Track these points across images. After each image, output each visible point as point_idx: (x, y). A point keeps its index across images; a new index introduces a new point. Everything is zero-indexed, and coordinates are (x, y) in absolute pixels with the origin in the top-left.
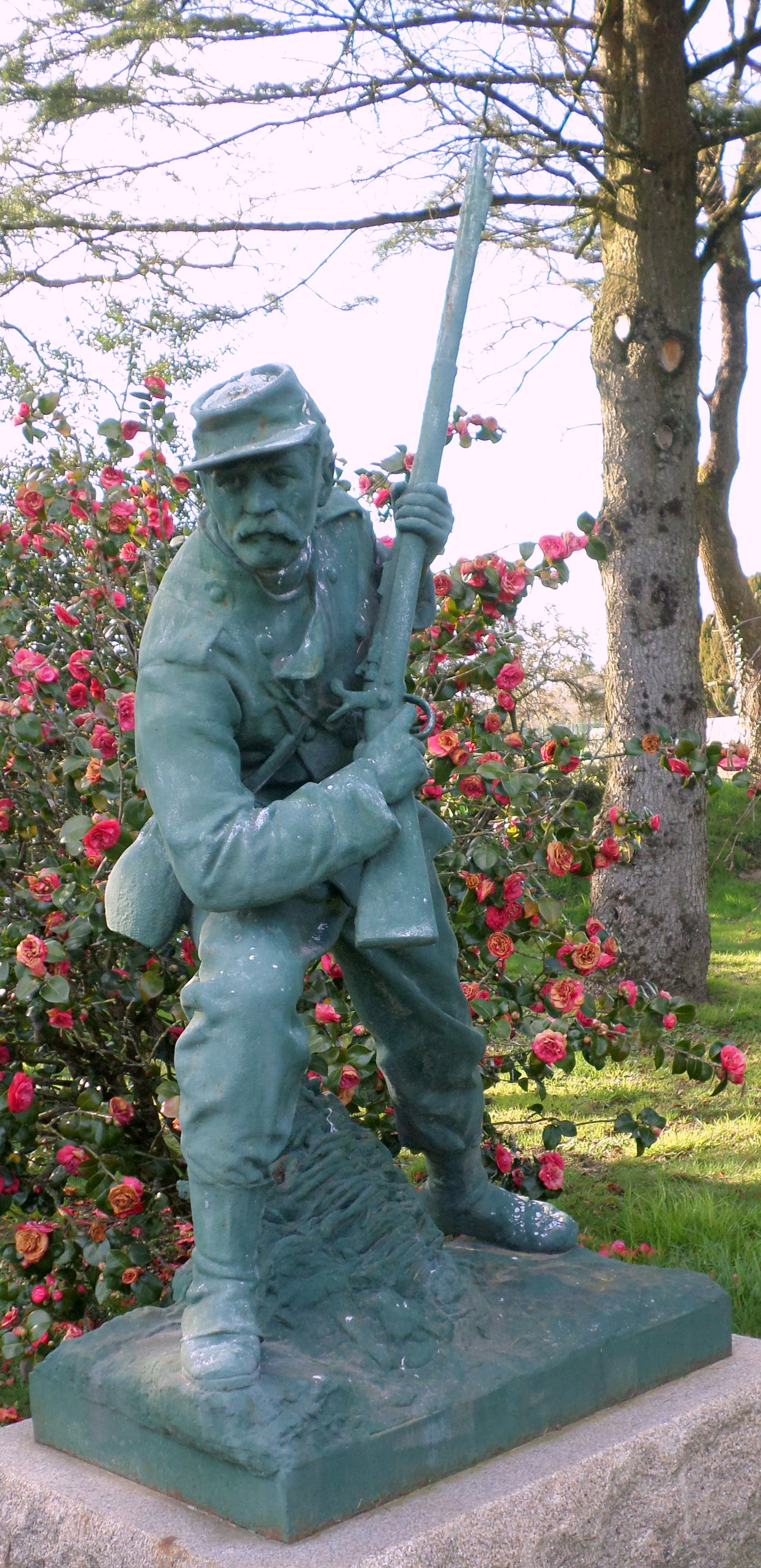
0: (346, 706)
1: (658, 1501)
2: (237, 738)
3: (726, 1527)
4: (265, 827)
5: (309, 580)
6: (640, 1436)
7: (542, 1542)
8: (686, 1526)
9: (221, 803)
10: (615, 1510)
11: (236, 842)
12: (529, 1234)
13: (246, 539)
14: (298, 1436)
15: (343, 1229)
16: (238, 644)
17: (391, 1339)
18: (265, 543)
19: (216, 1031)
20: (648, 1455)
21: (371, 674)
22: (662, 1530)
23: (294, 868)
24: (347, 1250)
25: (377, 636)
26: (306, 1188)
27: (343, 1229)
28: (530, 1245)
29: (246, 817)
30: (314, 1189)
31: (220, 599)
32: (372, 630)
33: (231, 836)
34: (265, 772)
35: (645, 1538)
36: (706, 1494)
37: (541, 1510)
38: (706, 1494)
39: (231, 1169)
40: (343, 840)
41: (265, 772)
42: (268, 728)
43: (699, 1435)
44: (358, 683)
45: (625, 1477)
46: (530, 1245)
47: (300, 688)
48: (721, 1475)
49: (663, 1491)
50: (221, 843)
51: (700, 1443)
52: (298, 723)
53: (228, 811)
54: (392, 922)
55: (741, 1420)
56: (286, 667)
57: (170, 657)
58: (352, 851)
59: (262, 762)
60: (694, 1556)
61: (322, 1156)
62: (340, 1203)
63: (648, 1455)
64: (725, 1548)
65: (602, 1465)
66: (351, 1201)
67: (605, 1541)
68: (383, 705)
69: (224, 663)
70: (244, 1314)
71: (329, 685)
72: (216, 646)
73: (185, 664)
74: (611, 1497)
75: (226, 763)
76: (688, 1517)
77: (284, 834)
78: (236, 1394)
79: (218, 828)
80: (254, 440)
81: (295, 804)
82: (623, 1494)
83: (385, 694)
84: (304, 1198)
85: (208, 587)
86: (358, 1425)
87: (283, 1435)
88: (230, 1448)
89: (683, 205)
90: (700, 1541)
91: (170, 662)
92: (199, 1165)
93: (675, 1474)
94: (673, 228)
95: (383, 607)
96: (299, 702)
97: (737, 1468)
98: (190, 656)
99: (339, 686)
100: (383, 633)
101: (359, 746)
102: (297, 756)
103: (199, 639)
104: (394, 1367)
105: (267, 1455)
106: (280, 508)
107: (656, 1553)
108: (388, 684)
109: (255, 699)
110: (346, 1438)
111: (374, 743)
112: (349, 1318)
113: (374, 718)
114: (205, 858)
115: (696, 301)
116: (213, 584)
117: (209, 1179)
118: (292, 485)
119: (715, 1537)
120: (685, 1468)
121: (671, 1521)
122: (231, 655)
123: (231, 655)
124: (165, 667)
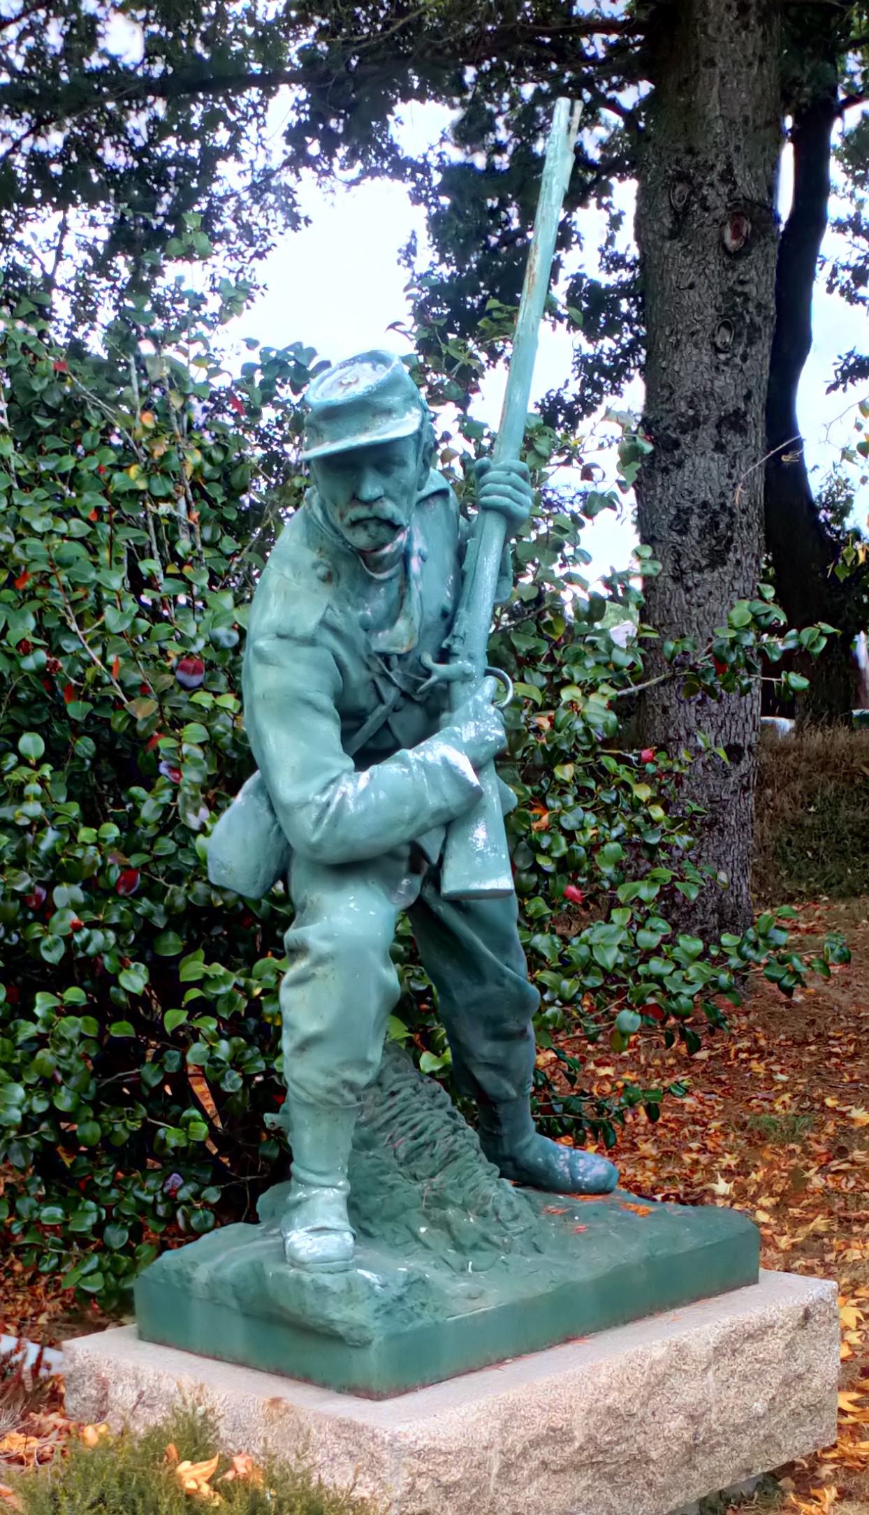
0: (434, 678)
1: (689, 1393)
2: (336, 706)
3: (748, 1424)
4: (366, 790)
5: (405, 557)
6: (675, 1337)
7: (590, 1412)
8: (714, 1417)
9: (328, 768)
10: (651, 1395)
11: (342, 804)
12: (573, 1179)
13: (355, 523)
14: (388, 1313)
15: (414, 1154)
16: (339, 621)
17: (459, 1247)
18: (373, 528)
19: (320, 970)
20: (681, 1352)
21: (456, 647)
22: (692, 1417)
23: (392, 825)
24: (419, 1173)
25: (462, 611)
26: (382, 1120)
27: (414, 1154)
28: (576, 1190)
29: (350, 780)
30: (387, 1122)
31: (327, 579)
32: (456, 603)
33: (338, 797)
34: (360, 738)
35: (676, 1423)
36: (732, 1392)
37: (591, 1387)
38: (732, 1392)
39: (331, 1091)
40: (433, 802)
41: (360, 738)
42: (364, 699)
43: (727, 1340)
44: (444, 656)
45: (660, 1369)
46: (576, 1190)
47: (394, 660)
48: (745, 1378)
49: (694, 1384)
50: (328, 804)
51: (727, 1348)
52: (390, 695)
53: (334, 775)
54: (473, 878)
55: (765, 1333)
56: (382, 641)
57: (284, 632)
58: (439, 812)
59: (358, 729)
60: (719, 1444)
61: (393, 1094)
62: (410, 1134)
63: (681, 1352)
64: (746, 1442)
65: (644, 1357)
66: (421, 1133)
67: (643, 1420)
68: (466, 677)
69: (329, 638)
70: (341, 1217)
71: (419, 659)
72: (324, 623)
73: (296, 639)
74: (648, 1383)
75: (329, 730)
76: (715, 1409)
77: (382, 795)
78: (338, 1276)
79: (324, 789)
80: (366, 430)
81: (388, 770)
82: (658, 1383)
83: (468, 665)
84: (379, 1129)
85: (315, 566)
86: (436, 1310)
87: (377, 1310)
88: (332, 1321)
89: (764, 35)
90: (725, 1432)
91: (281, 636)
92: (303, 1088)
93: (705, 1370)
94: (750, 65)
95: (468, 583)
96: (392, 675)
97: (761, 1373)
98: (299, 632)
99: (428, 660)
100: (468, 609)
101: (445, 716)
102: (386, 725)
103: (308, 617)
104: (463, 1270)
105: (364, 1327)
106: (387, 495)
107: (686, 1436)
108: (471, 658)
109: (357, 674)
110: (426, 1319)
111: (459, 713)
112: (423, 1230)
113: (459, 690)
114: (314, 816)
115: (775, 165)
116: (320, 563)
117: (311, 1100)
118: (398, 473)
119: (737, 1430)
120: (714, 1367)
121: (700, 1410)
122: (335, 631)
123: (335, 631)
124: (277, 642)
